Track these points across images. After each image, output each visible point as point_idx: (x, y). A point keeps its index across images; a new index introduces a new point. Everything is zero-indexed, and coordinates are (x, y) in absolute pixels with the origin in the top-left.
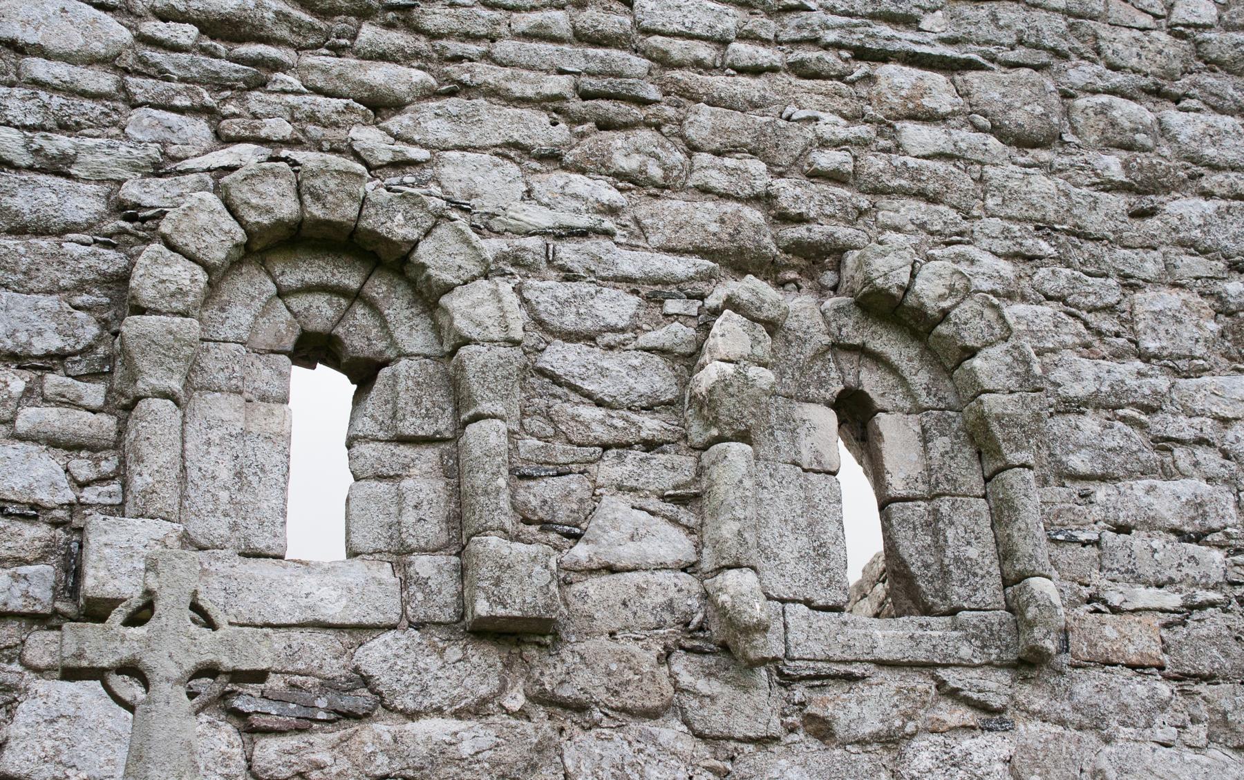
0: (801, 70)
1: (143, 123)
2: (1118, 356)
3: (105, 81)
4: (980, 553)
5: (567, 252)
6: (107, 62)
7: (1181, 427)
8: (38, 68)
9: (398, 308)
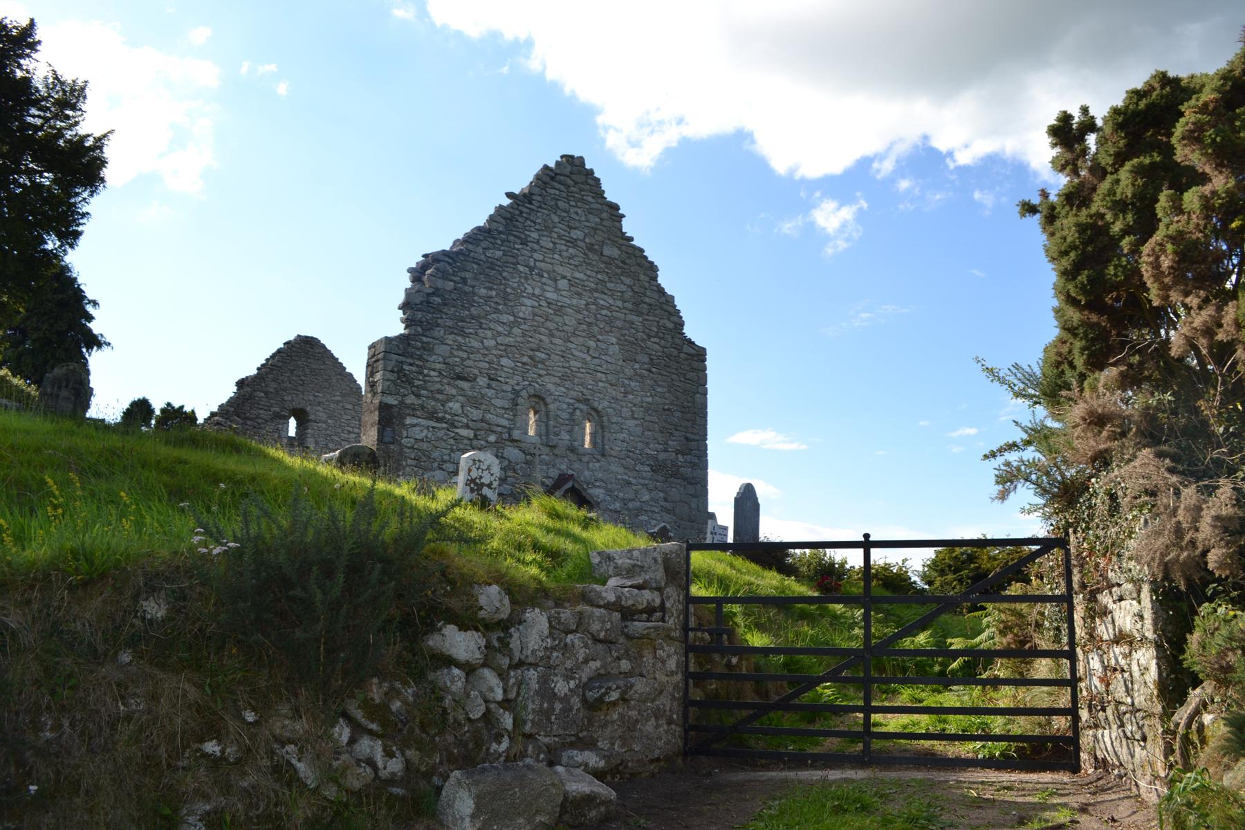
1: (516, 377)
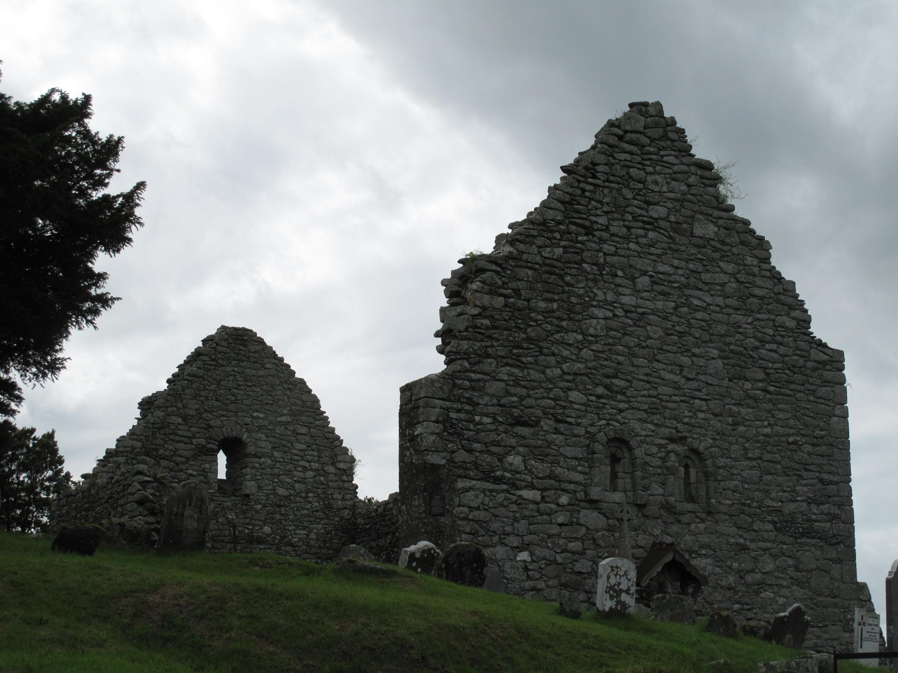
0: (682, 401)
2: (727, 458)
3: (583, 408)
4: (703, 494)
5: (648, 439)
7: (735, 472)
8: (576, 406)
9: (625, 450)
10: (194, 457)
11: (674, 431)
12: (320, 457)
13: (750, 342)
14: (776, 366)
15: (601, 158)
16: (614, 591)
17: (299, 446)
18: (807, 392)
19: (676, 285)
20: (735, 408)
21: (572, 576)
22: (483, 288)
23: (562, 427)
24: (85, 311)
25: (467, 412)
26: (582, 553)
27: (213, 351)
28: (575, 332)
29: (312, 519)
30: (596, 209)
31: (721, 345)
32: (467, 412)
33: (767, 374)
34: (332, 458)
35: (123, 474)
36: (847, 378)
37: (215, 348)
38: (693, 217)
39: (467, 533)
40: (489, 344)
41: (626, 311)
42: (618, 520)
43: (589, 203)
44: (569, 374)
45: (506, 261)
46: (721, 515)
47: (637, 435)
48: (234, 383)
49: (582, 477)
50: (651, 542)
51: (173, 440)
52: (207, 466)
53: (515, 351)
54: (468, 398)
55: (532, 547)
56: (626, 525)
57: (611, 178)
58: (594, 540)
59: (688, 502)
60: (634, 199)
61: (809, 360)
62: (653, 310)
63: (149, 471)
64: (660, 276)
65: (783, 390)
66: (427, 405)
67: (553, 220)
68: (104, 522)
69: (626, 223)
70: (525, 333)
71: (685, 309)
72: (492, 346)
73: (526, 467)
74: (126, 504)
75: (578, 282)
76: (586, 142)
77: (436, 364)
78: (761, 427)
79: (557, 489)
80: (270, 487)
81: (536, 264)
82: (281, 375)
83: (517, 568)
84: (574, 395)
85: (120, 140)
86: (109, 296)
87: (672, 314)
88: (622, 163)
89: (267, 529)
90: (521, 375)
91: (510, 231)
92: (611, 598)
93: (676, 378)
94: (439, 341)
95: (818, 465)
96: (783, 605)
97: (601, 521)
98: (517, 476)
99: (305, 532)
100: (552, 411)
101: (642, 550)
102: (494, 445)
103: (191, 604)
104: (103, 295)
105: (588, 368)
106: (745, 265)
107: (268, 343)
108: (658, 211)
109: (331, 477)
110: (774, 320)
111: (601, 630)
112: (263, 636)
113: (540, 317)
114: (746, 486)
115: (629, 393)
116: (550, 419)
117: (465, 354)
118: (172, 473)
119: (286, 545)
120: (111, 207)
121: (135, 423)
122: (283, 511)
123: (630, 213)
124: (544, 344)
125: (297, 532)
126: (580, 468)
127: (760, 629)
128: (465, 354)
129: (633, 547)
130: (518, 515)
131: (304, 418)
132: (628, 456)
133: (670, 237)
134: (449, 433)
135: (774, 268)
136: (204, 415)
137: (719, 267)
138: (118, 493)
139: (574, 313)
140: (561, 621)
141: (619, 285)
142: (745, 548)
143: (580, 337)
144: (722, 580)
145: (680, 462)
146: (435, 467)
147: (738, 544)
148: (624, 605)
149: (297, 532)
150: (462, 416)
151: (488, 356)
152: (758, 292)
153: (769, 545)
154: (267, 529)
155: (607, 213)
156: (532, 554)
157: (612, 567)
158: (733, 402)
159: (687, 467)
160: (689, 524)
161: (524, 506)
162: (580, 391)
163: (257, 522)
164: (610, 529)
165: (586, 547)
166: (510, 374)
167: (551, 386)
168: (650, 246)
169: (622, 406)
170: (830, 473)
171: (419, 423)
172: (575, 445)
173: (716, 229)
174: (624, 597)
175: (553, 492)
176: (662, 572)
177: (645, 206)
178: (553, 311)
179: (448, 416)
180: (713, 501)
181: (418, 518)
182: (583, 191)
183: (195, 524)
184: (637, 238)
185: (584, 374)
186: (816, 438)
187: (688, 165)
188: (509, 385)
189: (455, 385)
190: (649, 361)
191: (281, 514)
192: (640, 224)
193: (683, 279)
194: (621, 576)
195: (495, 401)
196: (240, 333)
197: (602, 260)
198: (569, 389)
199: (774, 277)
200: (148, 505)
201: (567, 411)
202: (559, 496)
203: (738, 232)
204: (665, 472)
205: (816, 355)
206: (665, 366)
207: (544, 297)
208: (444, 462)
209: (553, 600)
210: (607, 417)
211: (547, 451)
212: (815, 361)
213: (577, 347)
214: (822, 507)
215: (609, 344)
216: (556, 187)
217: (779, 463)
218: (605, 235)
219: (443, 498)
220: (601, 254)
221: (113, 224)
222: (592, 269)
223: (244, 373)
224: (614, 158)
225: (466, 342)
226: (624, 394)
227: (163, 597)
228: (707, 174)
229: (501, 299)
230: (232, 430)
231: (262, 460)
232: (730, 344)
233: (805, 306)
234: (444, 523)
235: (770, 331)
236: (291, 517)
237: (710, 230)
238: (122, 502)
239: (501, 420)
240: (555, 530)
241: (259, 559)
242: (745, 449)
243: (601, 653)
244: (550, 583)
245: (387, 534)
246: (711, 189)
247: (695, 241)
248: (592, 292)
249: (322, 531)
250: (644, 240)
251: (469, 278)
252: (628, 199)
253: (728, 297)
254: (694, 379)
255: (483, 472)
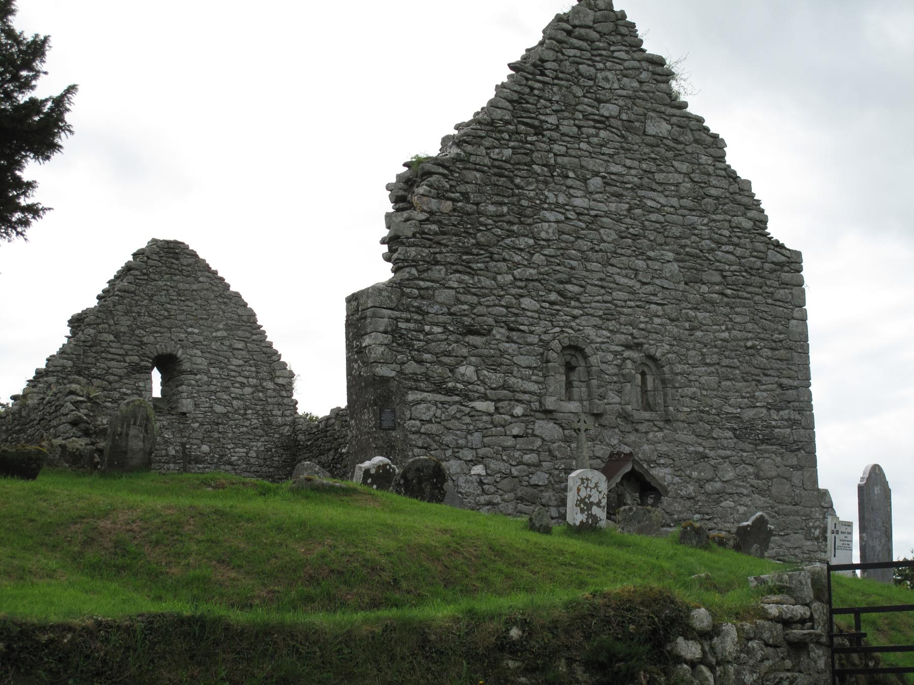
0: (638, 306)
2: (685, 364)
3: (536, 315)
4: (661, 401)
5: (603, 346)
6: (536, 312)
8: (529, 314)
9: (580, 358)
10: (128, 375)
11: (630, 338)
12: (257, 372)
13: (706, 243)
14: (733, 268)
15: (550, 55)
16: (585, 504)
17: (235, 362)
18: (765, 295)
19: (629, 186)
20: (692, 313)
21: (530, 490)
22: (430, 192)
23: (515, 335)
24: (15, 223)
25: (416, 321)
26: (538, 465)
27: (144, 265)
28: (526, 236)
29: (251, 437)
30: (546, 108)
31: (676, 247)
32: (416, 321)
33: (724, 277)
34: (270, 373)
35: (55, 394)
36: (805, 279)
37: (146, 262)
38: (645, 115)
39: (419, 447)
40: (437, 250)
41: (578, 214)
42: (575, 430)
43: (538, 101)
44: (521, 280)
45: (454, 163)
46: (680, 423)
47: (592, 342)
48: (166, 300)
49: (536, 386)
50: (608, 453)
51: (106, 359)
52: (141, 384)
53: (464, 257)
54: (418, 307)
55: (487, 461)
56: (583, 435)
57: (561, 75)
58: (550, 451)
59: (646, 410)
60: (584, 96)
61: (766, 262)
62: (606, 212)
63: (82, 391)
64: (613, 177)
65: (740, 293)
66: (374, 315)
67: (501, 120)
68: (44, 444)
69: (577, 122)
70: (475, 238)
71: (638, 211)
72: (441, 253)
73: (478, 378)
74: (58, 425)
75: (529, 184)
76: (534, 38)
77: (384, 273)
78: (718, 331)
79: (511, 400)
80: (207, 405)
81: (485, 166)
82: (216, 289)
83: (472, 482)
84: (527, 302)
85: (46, 39)
86: (40, 207)
87: (626, 216)
88: (571, 59)
89: (205, 448)
90: (471, 282)
91: (456, 132)
92: (582, 511)
93: (631, 283)
94: (385, 248)
95: (778, 370)
96: (743, 514)
97: (557, 432)
98: (470, 387)
99: (245, 450)
100: (504, 319)
101: (599, 461)
102: (445, 355)
103: (144, 529)
104: (34, 205)
105: (541, 274)
106: (700, 164)
107: (201, 256)
108: (609, 109)
109: (270, 392)
110: (730, 221)
111: (576, 545)
112: (223, 561)
113: (490, 221)
114: (705, 393)
115: (583, 299)
116: (502, 327)
117: (413, 261)
118: (106, 392)
119: (226, 463)
120: (39, 112)
121: (65, 341)
122: (221, 429)
123: (581, 112)
124: (495, 250)
125: (237, 450)
126: (534, 378)
127: (728, 540)
128: (413, 261)
129: (591, 458)
130: (471, 427)
131: (240, 333)
132: (583, 364)
133: (623, 136)
134: (398, 344)
135: (729, 166)
136: (137, 332)
137: (673, 166)
138: (50, 414)
139: (525, 216)
140: (534, 537)
141: (571, 187)
142: (704, 457)
143: (531, 242)
144: (681, 490)
145: (636, 369)
146: (385, 380)
147: (697, 453)
148: (595, 519)
149: (237, 450)
150: (412, 326)
151: (437, 263)
152: (713, 192)
153: (729, 453)
154: (205, 448)
155: (556, 111)
156: (486, 467)
157: (582, 479)
158: (690, 306)
159: (643, 374)
160: (647, 433)
161: (476, 418)
162: (532, 298)
163: (195, 441)
164: (567, 440)
165: (542, 459)
166: (460, 282)
167: (502, 293)
168: (602, 146)
169: (576, 312)
170: (789, 378)
171: (366, 334)
172: (529, 354)
173: (669, 127)
174: (595, 510)
175: (506, 402)
176: (621, 483)
177: (596, 104)
178: (503, 215)
179: (397, 326)
180: (671, 408)
181: (368, 433)
182: (532, 89)
183: (141, 444)
184: (588, 137)
185: (536, 280)
186: (775, 342)
187: (639, 61)
188: (459, 293)
189: (403, 294)
190: (603, 265)
191: (220, 433)
192: (591, 123)
193: (636, 179)
194: (591, 488)
195: (445, 310)
196: (171, 245)
197: (552, 161)
198: (522, 296)
199: (730, 177)
200: (82, 426)
201: (519, 319)
202: (513, 407)
203: (691, 130)
204: (622, 380)
205: (773, 256)
206: (619, 270)
207: (493, 200)
208: (393, 374)
209: (509, 515)
210: (561, 324)
211: (499, 360)
212: (773, 263)
213: (529, 252)
214: (781, 413)
215: (562, 249)
216: (503, 86)
217: (737, 368)
218: (555, 135)
219: (394, 411)
220: (551, 155)
221: (41, 130)
222: (543, 170)
223: (176, 287)
224: (563, 54)
225: (413, 249)
226: (578, 300)
227: (114, 523)
228: (659, 69)
229: (449, 203)
230: (166, 347)
231: (198, 377)
232: (686, 246)
233: (762, 206)
234: (395, 437)
235: (726, 233)
236: (230, 435)
237: (664, 128)
238: (54, 423)
239: (452, 329)
240: (510, 442)
241: (212, 480)
242: (703, 355)
243: (579, 570)
244: (506, 497)
245: (329, 450)
246: (663, 86)
247: (648, 139)
248: (543, 194)
249: (262, 449)
250: (595, 140)
251: (415, 182)
252: (579, 97)
253: (682, 198)
254: (649, 283)
255: (434, 384)
